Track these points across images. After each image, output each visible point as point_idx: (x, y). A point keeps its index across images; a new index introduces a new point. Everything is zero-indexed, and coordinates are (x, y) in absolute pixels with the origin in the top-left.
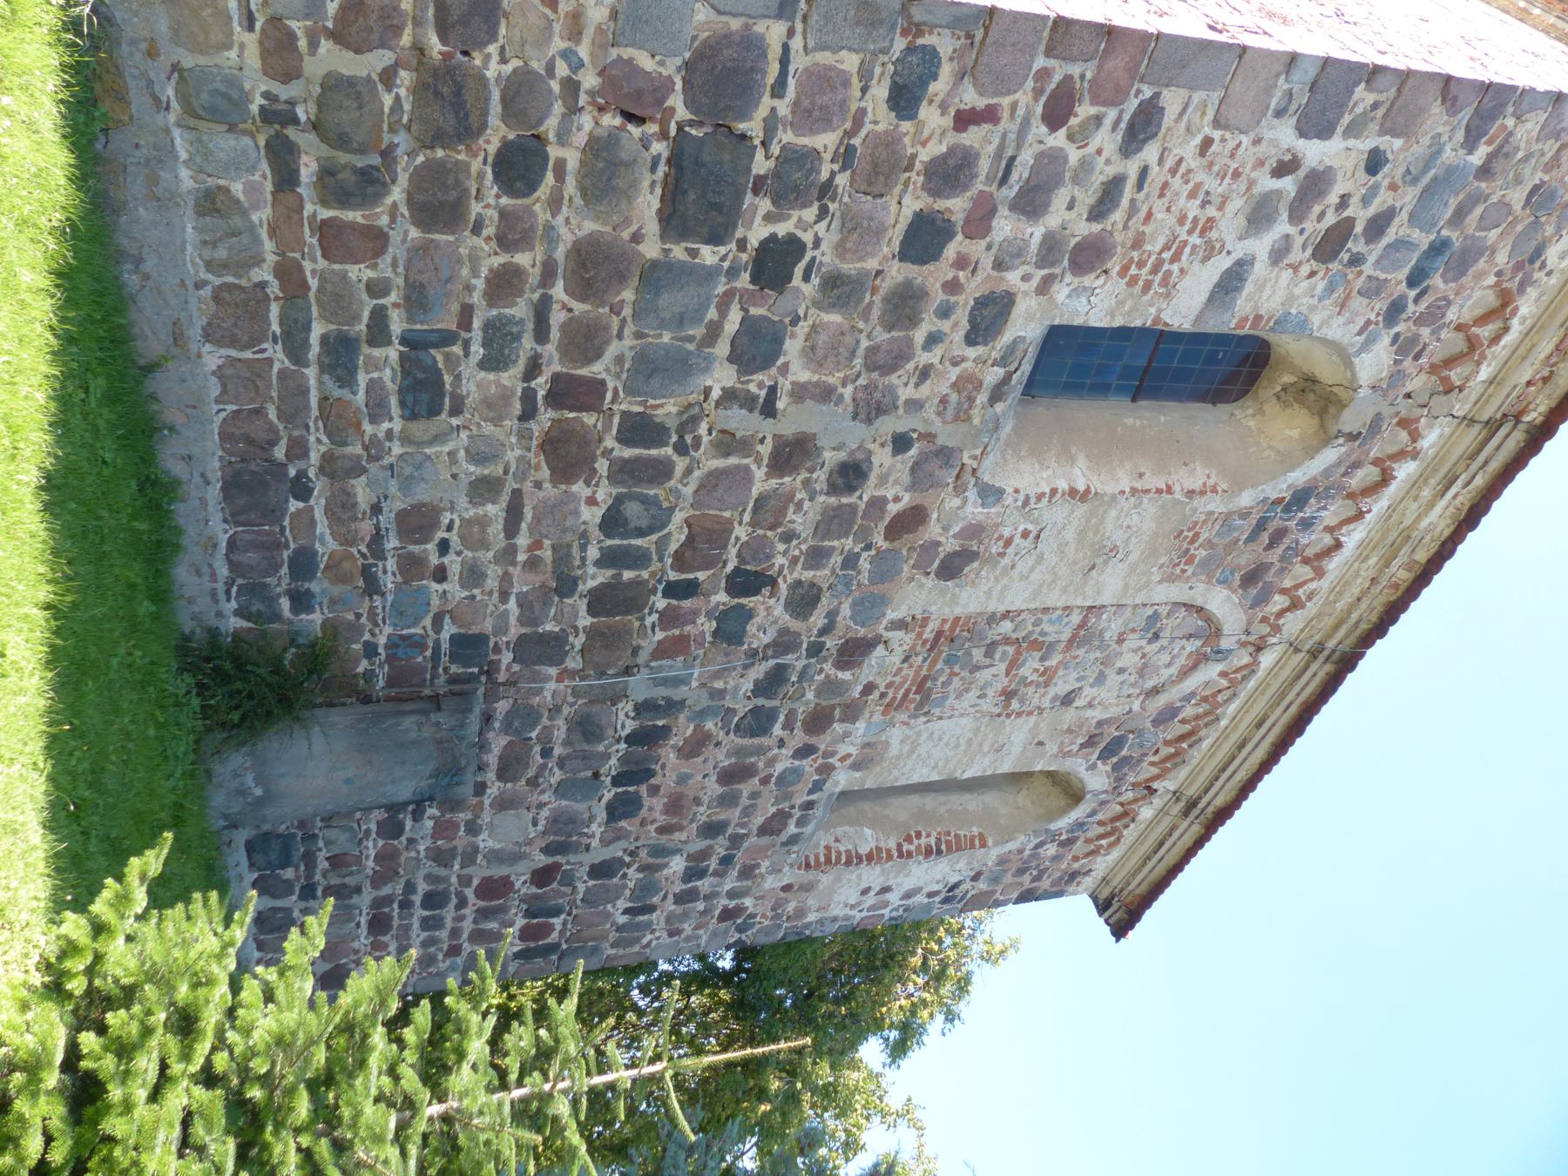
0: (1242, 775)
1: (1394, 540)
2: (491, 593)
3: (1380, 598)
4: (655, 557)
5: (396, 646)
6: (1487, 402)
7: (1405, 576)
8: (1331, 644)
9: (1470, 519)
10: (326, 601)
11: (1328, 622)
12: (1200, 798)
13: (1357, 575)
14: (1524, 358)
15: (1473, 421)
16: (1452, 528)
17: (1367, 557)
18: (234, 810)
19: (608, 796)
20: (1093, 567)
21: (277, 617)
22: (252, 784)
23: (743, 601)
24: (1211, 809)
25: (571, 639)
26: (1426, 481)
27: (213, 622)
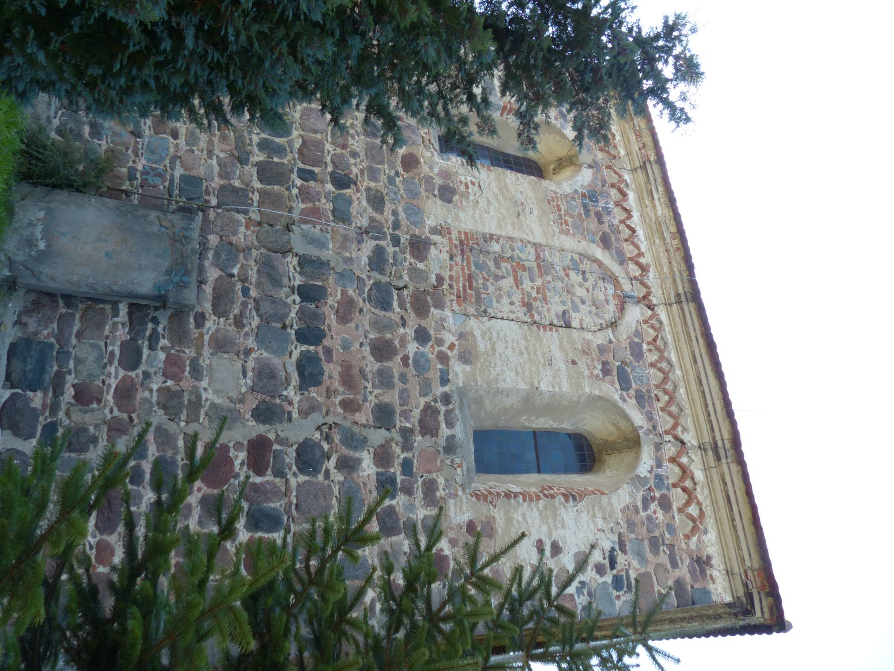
0: (719, 404)
1: (657, 228)
2: (202, 151)
3: (678, 257)
4: (288, 149)
5: (147, 173)
6: (633, 161)
7: (676, 242)
8: (681, 290)
9: (671, 201)
10: (110, 134)
11: (669, 282)
12: (714, 438)
13: (658, 252)
14: (629, 142)
15: (636, 169)
16: (671, 210)
17: (654, 241)
18: (16, 258)
19: (296, 354)
20: (519, 215)
21: (79, 136)
22: (39, 236)
23: (342, 191)
24: (728, 445)
25: (250, 195)
26: (643, 199)
27: (43, 122)
